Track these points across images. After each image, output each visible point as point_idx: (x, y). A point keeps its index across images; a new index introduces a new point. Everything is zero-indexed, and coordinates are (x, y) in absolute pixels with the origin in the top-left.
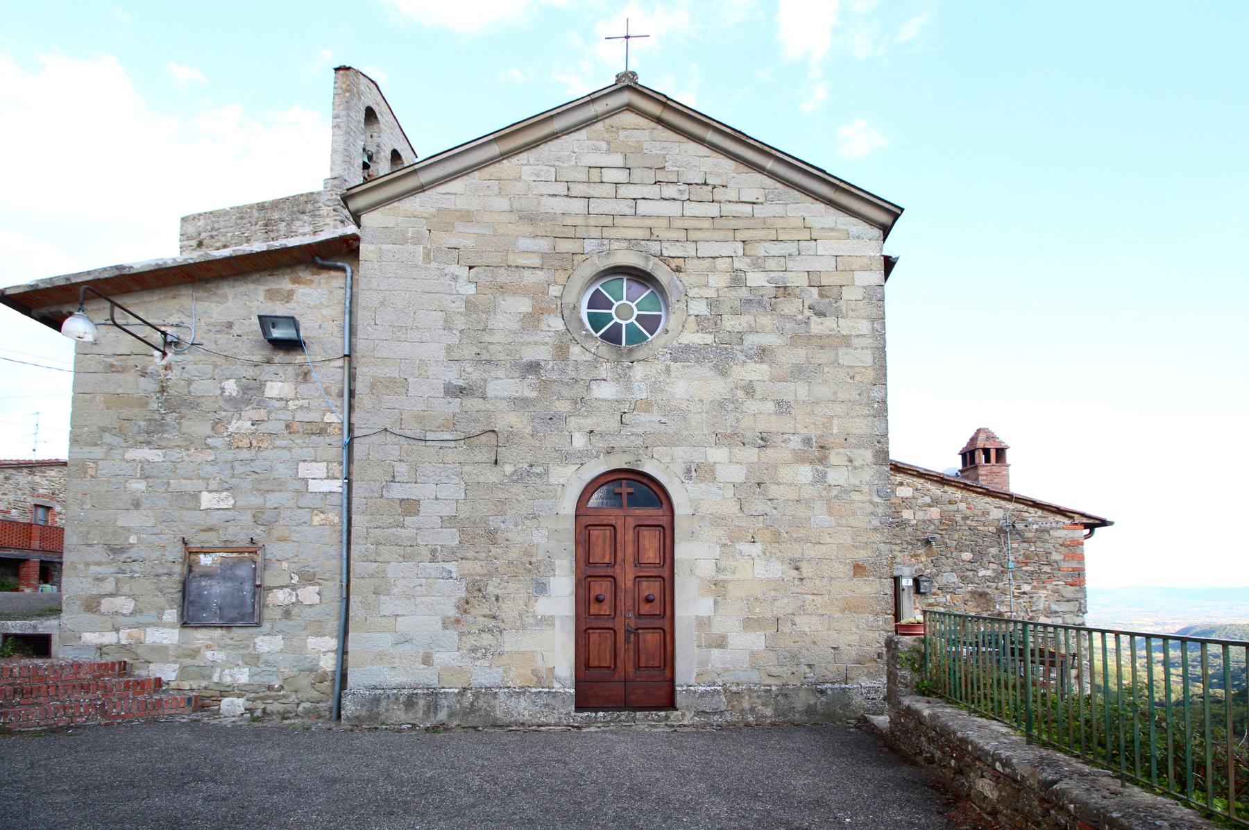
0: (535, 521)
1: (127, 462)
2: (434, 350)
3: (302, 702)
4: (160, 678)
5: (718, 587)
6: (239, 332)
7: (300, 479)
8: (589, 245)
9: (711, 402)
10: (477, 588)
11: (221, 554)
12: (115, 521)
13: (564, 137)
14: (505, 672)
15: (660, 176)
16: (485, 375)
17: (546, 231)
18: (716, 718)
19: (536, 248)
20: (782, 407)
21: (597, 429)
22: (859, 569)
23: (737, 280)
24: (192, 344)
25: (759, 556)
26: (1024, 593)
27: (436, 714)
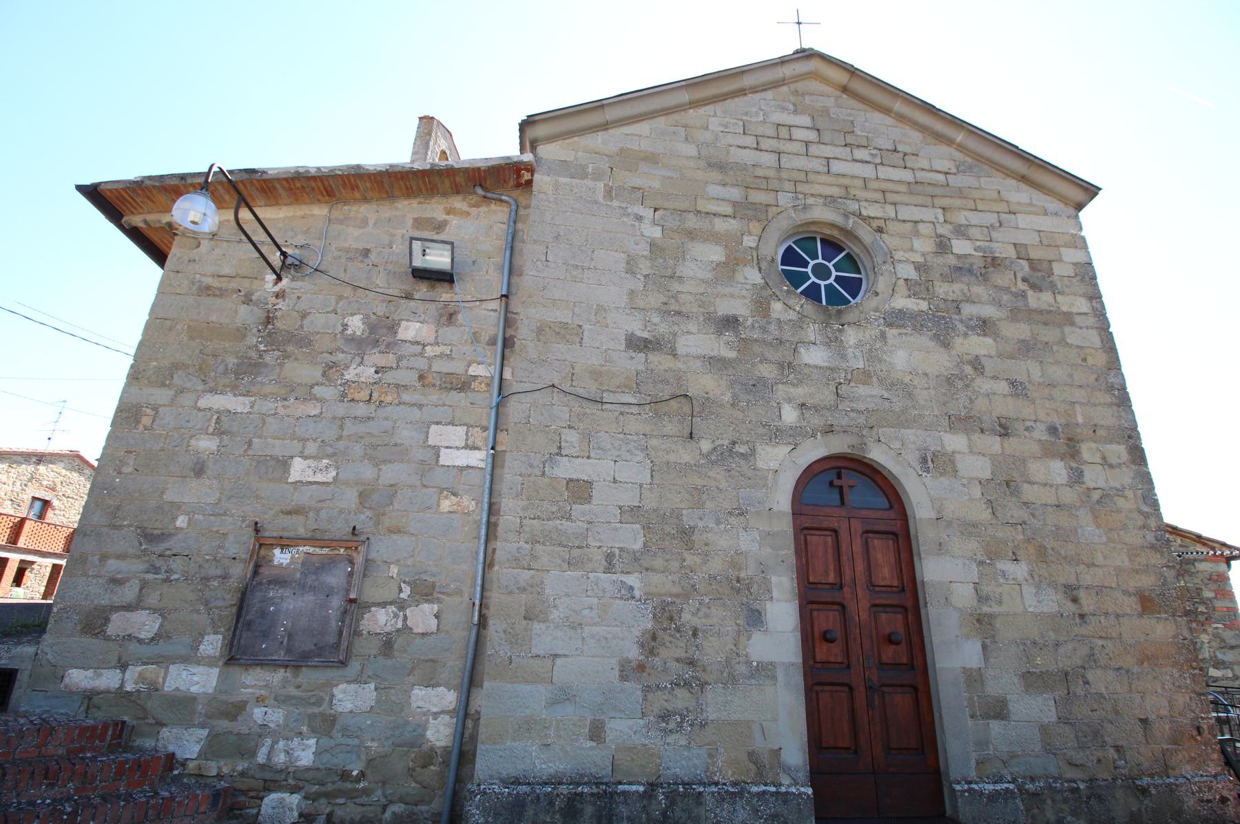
0: (742, 518)
1: (199, 410)
3: (392, 802)
4: (173, 754)
5: (982, 624)
9: (937, 377)
11: (307, 549)
12: (163, 493)
13: (750, 95)
14: (710, 756)
15: (850, 139)
16: (676, 328)
17: (737, 181)
19: (727, 196)
20: (1018, 388)
21: (810, 402)
23: (943, 246)
24: (316, 270)
25: (1027, 581)
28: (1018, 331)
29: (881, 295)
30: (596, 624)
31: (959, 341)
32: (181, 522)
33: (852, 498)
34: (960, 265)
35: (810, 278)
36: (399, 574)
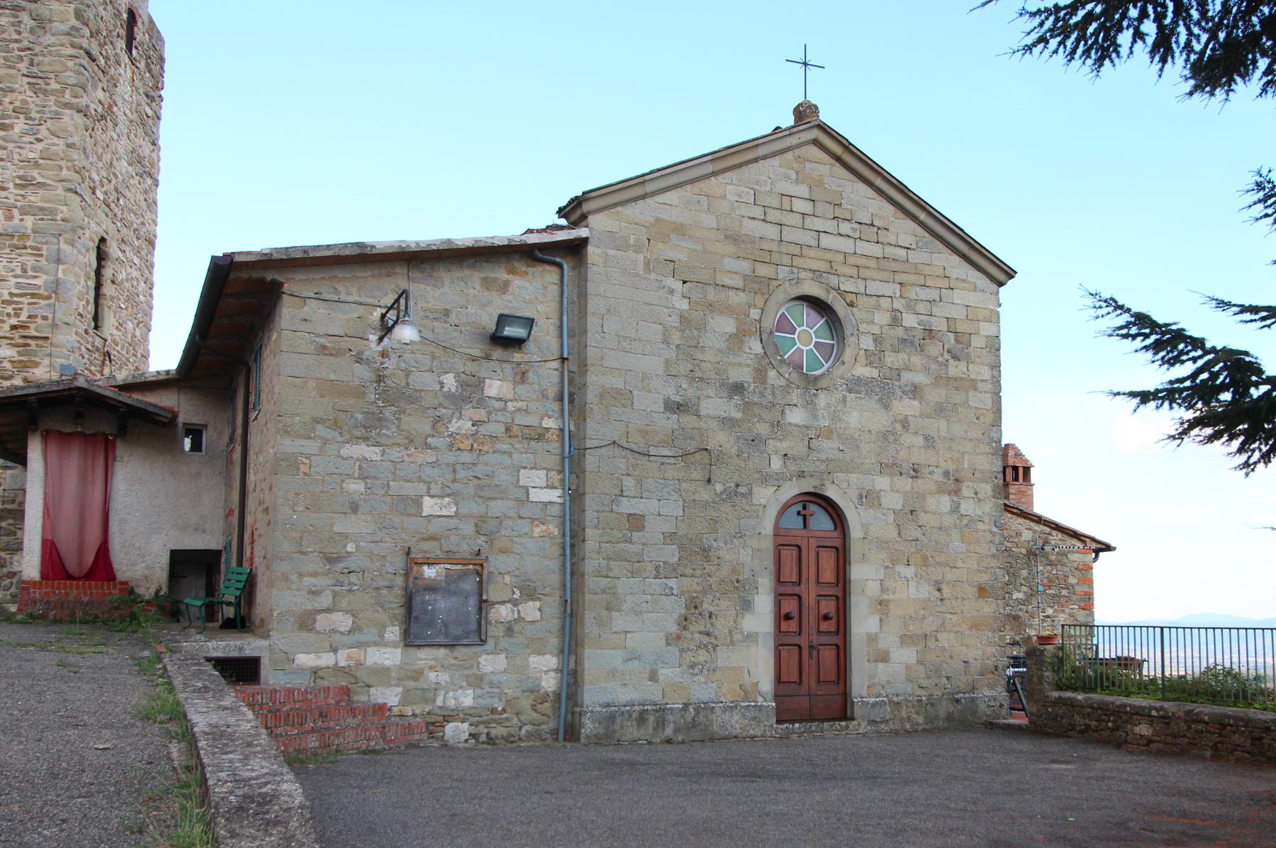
0: (741, 540)
1: (343, 459)
2: (653, 364)
3: (525, 724)
6: (457, 322)
7: (521, 487)
8: (783, 272)
10: (694, 605)
12: (332, 526)
16: (699, 393)
18: (883, 726)
20: (929, 441)
21: (791, 453)
22: (982, 591)
23: (896, 321)
26: (1048, 617)
27: (664, 729)
28: (936, 395)
29: (846, 364)
30: (652, 612)
31: (895, 403)
32: (350, 547)
33: (813, 523)
34: (906, 337)
35: (794, 334)
36: (511, 582)
